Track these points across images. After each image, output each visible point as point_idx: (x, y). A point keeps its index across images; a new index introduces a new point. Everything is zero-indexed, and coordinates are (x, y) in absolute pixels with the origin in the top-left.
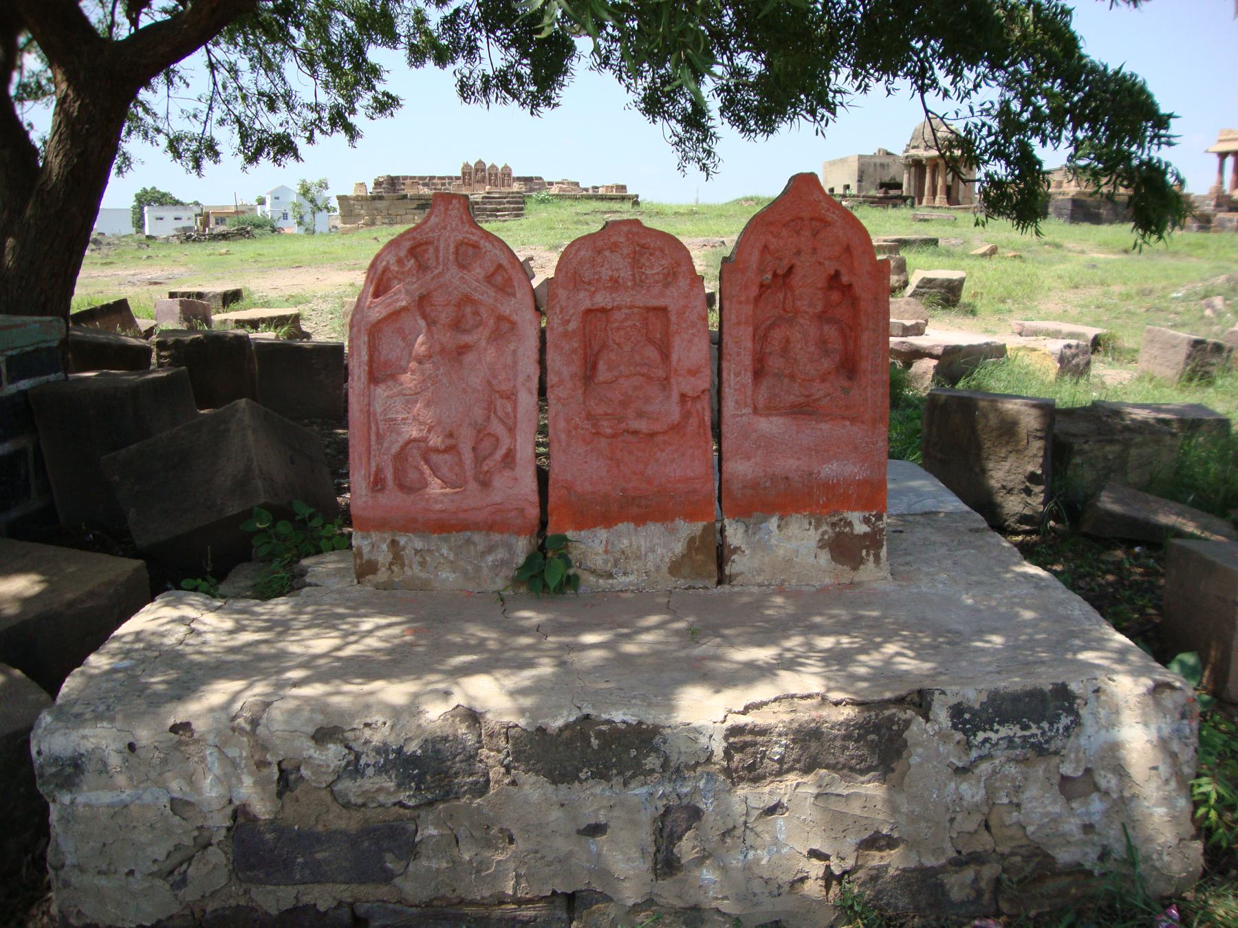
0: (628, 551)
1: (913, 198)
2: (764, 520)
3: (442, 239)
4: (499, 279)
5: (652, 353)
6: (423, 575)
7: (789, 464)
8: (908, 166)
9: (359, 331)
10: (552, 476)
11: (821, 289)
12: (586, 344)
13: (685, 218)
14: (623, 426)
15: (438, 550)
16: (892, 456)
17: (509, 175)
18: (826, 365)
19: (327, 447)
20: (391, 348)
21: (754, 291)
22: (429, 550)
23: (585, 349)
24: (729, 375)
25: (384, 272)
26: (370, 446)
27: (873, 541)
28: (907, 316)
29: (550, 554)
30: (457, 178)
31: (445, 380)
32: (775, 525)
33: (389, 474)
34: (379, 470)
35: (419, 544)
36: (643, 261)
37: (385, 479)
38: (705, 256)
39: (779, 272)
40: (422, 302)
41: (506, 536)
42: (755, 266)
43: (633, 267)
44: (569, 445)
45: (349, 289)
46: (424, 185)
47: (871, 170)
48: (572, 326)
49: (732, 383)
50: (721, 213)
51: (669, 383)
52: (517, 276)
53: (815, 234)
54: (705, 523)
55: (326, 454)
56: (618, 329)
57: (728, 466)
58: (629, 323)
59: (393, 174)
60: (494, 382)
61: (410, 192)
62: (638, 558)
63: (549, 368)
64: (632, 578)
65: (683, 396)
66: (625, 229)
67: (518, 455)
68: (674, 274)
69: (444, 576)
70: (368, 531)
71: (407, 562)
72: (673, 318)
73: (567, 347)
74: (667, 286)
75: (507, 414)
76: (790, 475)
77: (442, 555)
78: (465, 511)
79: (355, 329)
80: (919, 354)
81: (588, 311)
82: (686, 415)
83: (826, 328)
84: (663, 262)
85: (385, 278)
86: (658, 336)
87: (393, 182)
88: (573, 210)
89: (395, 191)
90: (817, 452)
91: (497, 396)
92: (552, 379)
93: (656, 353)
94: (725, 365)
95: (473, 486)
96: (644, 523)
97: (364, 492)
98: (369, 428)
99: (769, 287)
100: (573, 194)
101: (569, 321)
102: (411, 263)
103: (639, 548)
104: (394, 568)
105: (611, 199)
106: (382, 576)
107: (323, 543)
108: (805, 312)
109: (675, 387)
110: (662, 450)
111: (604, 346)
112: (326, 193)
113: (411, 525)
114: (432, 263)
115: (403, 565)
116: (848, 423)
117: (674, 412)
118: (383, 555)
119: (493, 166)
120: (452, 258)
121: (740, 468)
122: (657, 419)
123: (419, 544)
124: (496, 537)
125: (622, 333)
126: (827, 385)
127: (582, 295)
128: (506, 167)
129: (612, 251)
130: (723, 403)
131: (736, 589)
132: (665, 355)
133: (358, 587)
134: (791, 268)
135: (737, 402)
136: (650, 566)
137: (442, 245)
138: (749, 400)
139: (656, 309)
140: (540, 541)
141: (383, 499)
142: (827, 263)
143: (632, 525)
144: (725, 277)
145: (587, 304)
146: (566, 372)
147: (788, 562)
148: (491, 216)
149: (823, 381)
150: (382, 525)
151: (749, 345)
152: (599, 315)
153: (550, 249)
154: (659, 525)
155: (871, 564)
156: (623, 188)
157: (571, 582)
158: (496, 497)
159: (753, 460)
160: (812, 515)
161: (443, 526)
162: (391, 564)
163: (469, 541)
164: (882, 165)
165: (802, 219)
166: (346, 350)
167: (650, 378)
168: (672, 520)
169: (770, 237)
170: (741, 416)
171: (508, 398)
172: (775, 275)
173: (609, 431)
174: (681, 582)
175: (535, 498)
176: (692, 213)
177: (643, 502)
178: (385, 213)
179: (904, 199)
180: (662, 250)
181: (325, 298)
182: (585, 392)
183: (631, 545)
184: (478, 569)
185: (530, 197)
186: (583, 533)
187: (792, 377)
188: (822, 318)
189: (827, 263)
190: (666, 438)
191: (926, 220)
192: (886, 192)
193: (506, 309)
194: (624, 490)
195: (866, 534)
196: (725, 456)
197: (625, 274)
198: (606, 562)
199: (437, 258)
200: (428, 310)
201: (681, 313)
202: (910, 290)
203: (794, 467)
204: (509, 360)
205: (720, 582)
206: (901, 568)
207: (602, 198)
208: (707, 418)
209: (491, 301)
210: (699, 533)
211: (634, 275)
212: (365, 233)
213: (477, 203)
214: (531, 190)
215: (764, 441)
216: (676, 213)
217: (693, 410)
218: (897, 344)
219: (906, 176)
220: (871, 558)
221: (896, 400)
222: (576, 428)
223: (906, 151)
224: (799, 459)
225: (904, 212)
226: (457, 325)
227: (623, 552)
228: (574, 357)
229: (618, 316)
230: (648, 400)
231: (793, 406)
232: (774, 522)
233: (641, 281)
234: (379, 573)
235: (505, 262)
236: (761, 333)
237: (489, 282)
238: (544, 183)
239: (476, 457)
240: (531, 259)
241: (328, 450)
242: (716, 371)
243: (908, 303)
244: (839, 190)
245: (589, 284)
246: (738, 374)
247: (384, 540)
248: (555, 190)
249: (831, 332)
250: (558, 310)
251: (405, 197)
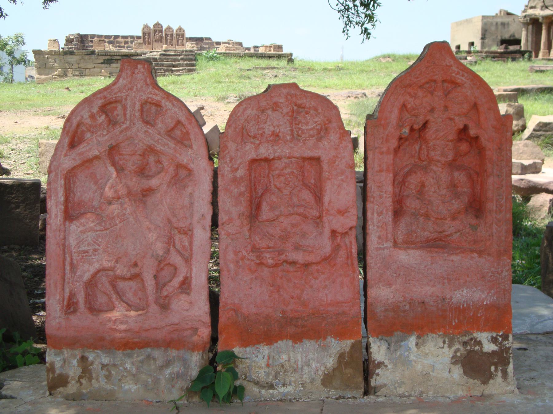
0: (287, 365)
1: (530, 52)
2: (404, 339)
3: (129, 98)
4: (178, 133)
5: (307, 196)
6: (109, 387)
7: (425, 291)
8: (526, 24)
9: (56, 175)
10: (222, 300)
11: (451, 141)
12: (252, 189)
13: (333, 72)
14: (283, 257)
15: (122, 364)
16: (514, 282)
17: (183, 35)
18: (456, 206)
19: (24, 270)
20: (85, 191)
21: (394, 143)
22: (114, 365)
23: (251, 193)
24: (373, 214)
25: (78, 126)
26: (64, 274)
27: (501, 358)
28: (525, 156)
29: (219, 368)
30: (139, 38)
31: (131, 219)
32: (414, 343)
33: (81, 298)
34: (72, 295)
35: (105, 360)
36: (300, 118)
37: (77, 303)
38: (349, 105)
39: (416, 127)
40: (113, 151)
41: (182, 352)
42: (394, 122)
43: (291, 123)
44: (236, 273)
45: (45, 132)
46: (110, 43)
47: (493, 28)
48: (240, 173)
49: (375, 221)
50: (363, 69)
51: (322, 221)
52: (192, 129)
53: (447, 94)
54: (353, 341)
55: (23, 277)
56: (279, 176)
57: (373, 292)
58: (288, 170)
59: (82, 33)
60: (174, 220)
61: (97, 49)
62: (296, 371)
63: (220, 208)
64: (290, 389)
65: (334, 232)
66: (285, 91)
67: (194, 282)
68: (326, 129)
69: (127, 387)
70: (61, 348)
71: (94, 375)
72: (325, 167)
73: (236, 190)
74: (319, 139)
75: (184, 247)
76: (427, 300)
77: (126, 369)
78: (147, 330)
79: (53, 174)
80: (537, 189)
81: (254, 161)
82: (336, 248)
83: (456, 174)
84: (316, 120)
85: (79, 131)
86: (313, 181)
87: (82, 39)
88: (237, 66)
89: (84, 47)
90: (449, 280)
91: (176, 232)
92: (222, 217)
93: (311, 196)
94: (369, 205)
95: (154, 308)
96: (301, 341)
97: (58, 314)
98: (64, 259)
99: (407, 139)
100: (237, 52)
101: (237, 169)
102: (102, 118)
103: (296, 362)
104: (83, 381)
105: (270, 57)
106: (72, 388)
107: (19, 358)
108: (438, 161)
109: (326, 225)
110: (316, 278)
111: (267, 190)
112: (23, 48)
113: (101, 343)
114: (120, 118)
115: (90, 379)
116: (476, 255)
117: (327, 247)
118: (73, 370)
119: (169, 28)
120: (137, 114)
121: (383, 294)
122: (312, 252)
123: (105, 360)
124: (173, 353)
125: (282, 179)
126: (457, 222)
127: (248, 147)
128: (180, 29)
129: (274, 110)
130: (368, 238)
131: (380, 399)
132: (318, 198)
133: (50, 398)
134: (425, 125)
135: (379, 237)
136: (306, 378)
137: (129, 103)
138: (390, 236)
139: (311, 159)
140: (211, 355)
141: (74, 320)
142: (456, 118)
143: (290, 343)
144: (369, 131)
145: (253, 155)
146: (235, 211)
147: (426, 376)
148: (167, 70)
149: (454, 218)
150: (73, 343)
151: (390, 189)
152: (263, 163)
153: (218, 100)
154: (313, 342)
155: (499, 379)
156: (280, 47)
157: (237, 392)
158: (174, 318)
159: (394, 287)
160: (446, 334)
161: (128, 345)
162: (80, 377)
163: (149, 357)
164: (503, 24)
165: (435, 81)
166: (44, 186)
167: (305, 217)
168: (325, 339)
169: (407, 97)
170: (384, 249)
171: (186, 233)
172: (412, 130)
173: (270, 261)
174: (332, 392)
175: (207, 319)
176: (338, 69)
177: (300, 322)
178: (75, 66)
179: (522, 53)
180: (316, 110)
181: (22, 139)
182: (250, 229)
183: (289, 360)
184: (157, 381)
185: (200, 55)
186: (248, 349)
187: (427, 216)
188: (453, 165)
189: (456, 118)
190: (319, 267)
191: (542, 71)
192: (506, 48)
193: (184, 158)
194: (283, 312)
195: (494, 352)
196: (370, 283)
197: (285, 129)
198: (268, 374)
199: (125, 114)
200: (117, 158)
201: (332, 162)
202: (527, 133)
203: (429, 293)
204: (187, 201)
205: (366, 393)
206: (527, 383)
207: (262, 56)
208: (354, 251)
209: (171, 152)
210: (347, 350)
211: (292, 130)
212: (58, 83)
213: (155, 60)
214: (202, 49)
215: (404, 271)
216: (325, 69)
217: (342, 244)
218: (516, 181)
219: (524, 34)
220: (500, 374)
221: (517, 230)
222: (243, 259)
223: (525, 11)
224: (433, 286)
225: (522, 64)
226: (142, 171)
227: (282, 366)
228: (243, 199)
229: (278, 164)
230: (304, 235)
231: (428, 241)
232: (412, 341)
233: (298, 135)
234: (70, 385)
235: (183, 119)
236: (400, 178)
237: (169, 136)
238: (212, 43)
239: (157, 284)
240: (202, 108)
241: (25, 274)
242: (361, 215)
243: (526, 145)
244: (465, 47)
245: (254, 137)
246: (380, 214)
247: (74, 356)
248: (222, 49)
249: (460, 177)
250: (228, 160)
251: (93, 53)
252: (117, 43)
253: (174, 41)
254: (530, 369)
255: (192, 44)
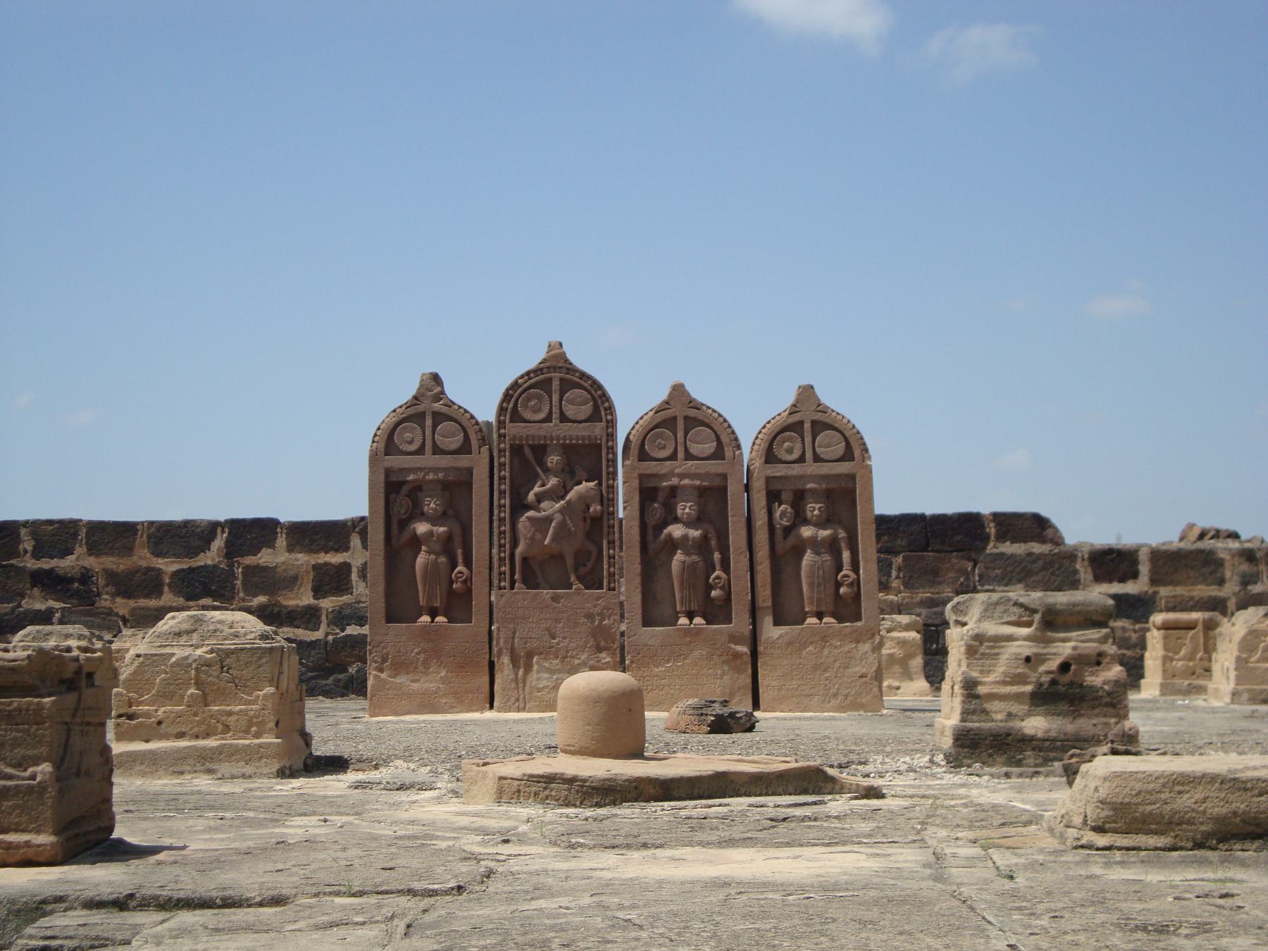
17: (844, 496)
119: (682, 417)
128: (808, 423)
252: (252, 590)
253: (740, 574)
254: (1236, 924)
255: (1053, 621)
